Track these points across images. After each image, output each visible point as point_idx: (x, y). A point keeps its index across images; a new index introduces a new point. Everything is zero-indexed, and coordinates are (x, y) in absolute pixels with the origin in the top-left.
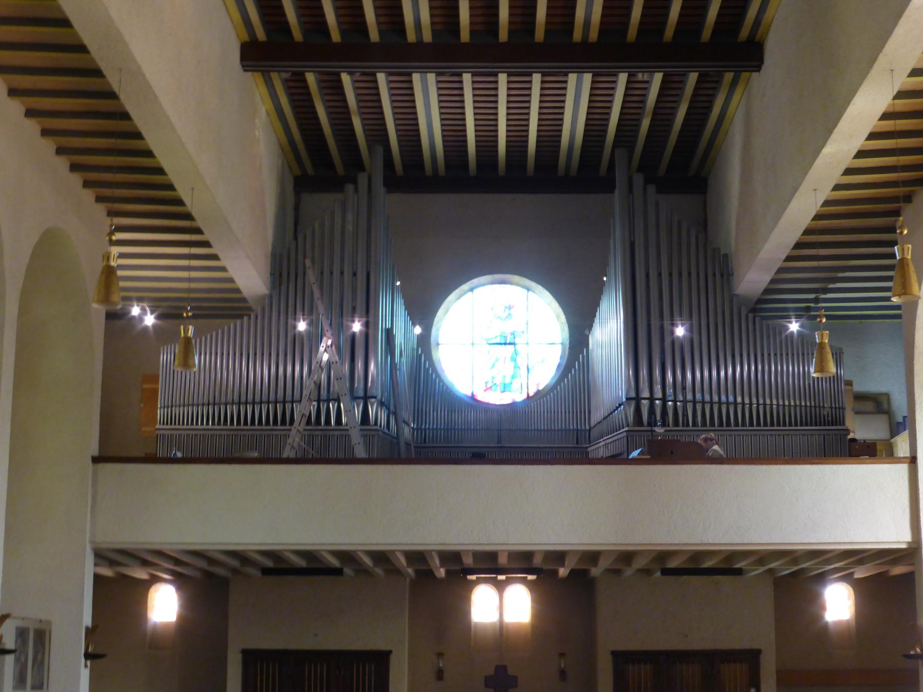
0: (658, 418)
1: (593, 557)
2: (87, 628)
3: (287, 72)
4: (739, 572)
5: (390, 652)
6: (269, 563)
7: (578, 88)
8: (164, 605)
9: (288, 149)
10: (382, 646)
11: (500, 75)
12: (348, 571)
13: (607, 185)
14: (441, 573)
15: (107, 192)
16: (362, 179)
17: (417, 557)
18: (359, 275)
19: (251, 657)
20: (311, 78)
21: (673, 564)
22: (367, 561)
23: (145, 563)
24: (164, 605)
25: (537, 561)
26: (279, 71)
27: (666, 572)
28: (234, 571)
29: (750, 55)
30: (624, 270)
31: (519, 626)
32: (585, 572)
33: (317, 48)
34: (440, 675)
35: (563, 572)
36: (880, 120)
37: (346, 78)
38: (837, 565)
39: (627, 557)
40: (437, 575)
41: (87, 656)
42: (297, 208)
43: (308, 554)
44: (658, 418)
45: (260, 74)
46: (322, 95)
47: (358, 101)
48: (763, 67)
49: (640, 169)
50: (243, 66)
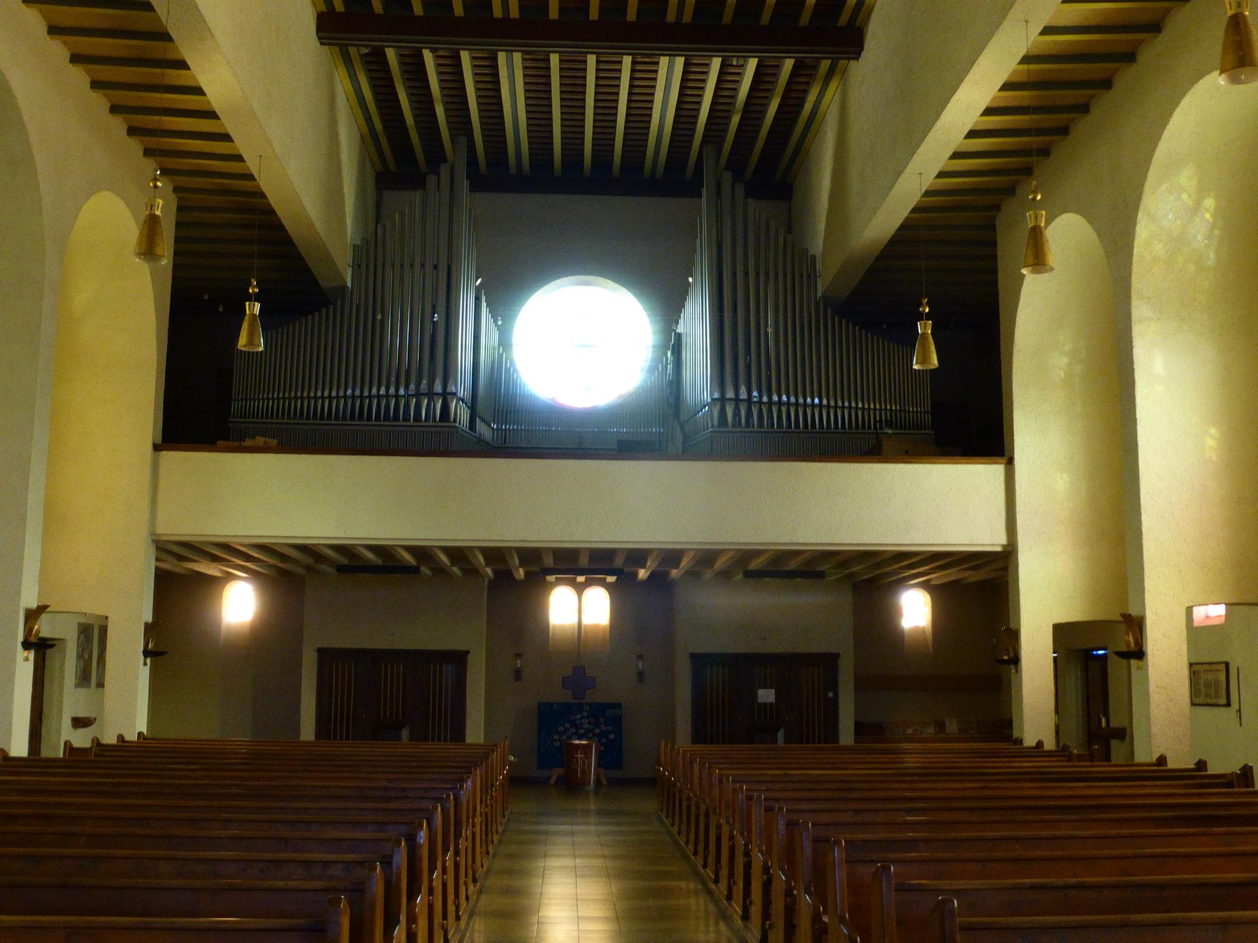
0: (743, 421)
1: (672, 557)
2: (147, 625)
3: (366, 46)
4: (821, 575)
5: (468, 652)
6: (344, 561)
7: (669, 71)
8: (239, 605)
9: (369, 140)
10: (458, 646)
11: (589, 56)
12: (425, 570)
13: (692, 189)
14: (520, 573)
15: (172, 163)
16: (444, 170)
17: (495, 555)
18: (440, 268)
19: (326, 655)
20: (391, 54)
21: (755, 565)
22: (444, 558)
23: (215, 559)
24: (239, 605)
25: (619, 562)
26: (357, 46)
27: (749, 574)
28: (308, 568)
29: (849, 41)
30: (710, 270)
31: (596, 628)
32: (665, 575)
33: (398, 23)
34: (518, 674)
35: (643, 574)
36: (983, 115)
37: (428, 56)
38: (921, 569)
39: (707, 557)
40: (516, 574)
41: (146, 653)
42: (378, 205)
43: (382, 551)
44: (743, 421)
45: (337, 49)
46: (405, 80)
47: (442, 88)
48: (863, 54)
49: (727, 169)
50: (320, 38)
